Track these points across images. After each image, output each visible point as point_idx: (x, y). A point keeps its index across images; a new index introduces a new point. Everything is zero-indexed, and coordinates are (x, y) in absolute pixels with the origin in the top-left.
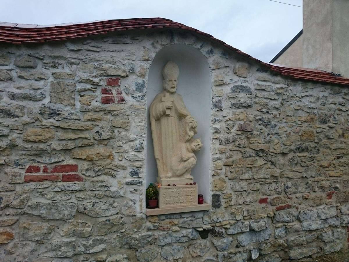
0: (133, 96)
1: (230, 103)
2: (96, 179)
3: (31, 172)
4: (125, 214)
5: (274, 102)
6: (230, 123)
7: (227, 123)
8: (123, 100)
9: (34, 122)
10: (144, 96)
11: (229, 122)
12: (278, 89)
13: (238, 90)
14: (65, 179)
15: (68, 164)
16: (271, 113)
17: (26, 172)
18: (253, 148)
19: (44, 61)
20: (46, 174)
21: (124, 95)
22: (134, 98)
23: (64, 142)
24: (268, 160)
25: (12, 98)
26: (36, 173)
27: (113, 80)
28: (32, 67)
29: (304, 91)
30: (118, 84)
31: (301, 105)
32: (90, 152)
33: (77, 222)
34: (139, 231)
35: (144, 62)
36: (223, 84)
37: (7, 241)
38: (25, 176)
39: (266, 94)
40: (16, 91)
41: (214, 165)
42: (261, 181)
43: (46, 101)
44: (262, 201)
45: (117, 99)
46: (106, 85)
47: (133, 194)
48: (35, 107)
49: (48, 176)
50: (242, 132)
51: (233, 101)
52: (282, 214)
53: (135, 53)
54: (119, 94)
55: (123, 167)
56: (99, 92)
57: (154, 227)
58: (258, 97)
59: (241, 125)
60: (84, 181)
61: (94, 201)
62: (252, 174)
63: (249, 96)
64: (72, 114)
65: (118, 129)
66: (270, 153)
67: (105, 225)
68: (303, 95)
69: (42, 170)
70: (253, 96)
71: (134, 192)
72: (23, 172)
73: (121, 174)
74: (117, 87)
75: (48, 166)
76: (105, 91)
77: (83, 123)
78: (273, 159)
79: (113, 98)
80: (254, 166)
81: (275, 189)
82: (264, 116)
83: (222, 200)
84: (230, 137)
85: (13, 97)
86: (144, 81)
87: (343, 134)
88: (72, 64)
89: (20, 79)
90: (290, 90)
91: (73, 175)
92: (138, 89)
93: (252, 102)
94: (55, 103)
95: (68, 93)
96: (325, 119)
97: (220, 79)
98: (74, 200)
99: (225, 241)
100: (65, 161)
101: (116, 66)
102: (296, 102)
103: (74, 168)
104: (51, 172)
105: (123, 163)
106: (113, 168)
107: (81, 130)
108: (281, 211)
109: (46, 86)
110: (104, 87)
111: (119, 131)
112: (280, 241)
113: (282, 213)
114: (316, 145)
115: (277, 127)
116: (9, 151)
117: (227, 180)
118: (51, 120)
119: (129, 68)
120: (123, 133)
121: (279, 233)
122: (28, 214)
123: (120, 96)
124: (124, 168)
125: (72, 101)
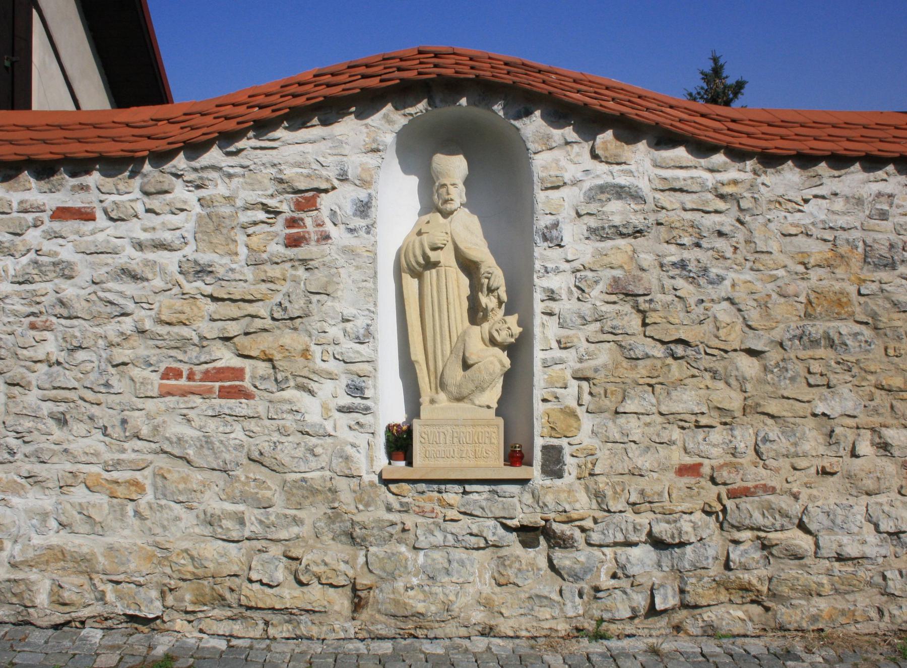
0: (349, 227)
1: (585, 227)
2: (279, 395)
3: (168, 379)
5: (716, 218)
6: (586, 276)
7: (578, 274)
8: (327, 237)
9: (170, 289)
10: (372, 225)
11: (583, 273)
12: (723, 184)
13: (604, 197)
14: (225, 393)
15: (228, 365)
16: (709, 246)
17: (162, 378)
18: (656, 337)
19: (185, 179)
20: (191, 383)
21: (329, 227)
22: (351, 231)
23: (219, 324)
24: (702, 368)
25: (138, 248)
26: (176, 379)
27: (305, 198)
28: (166, 192)
29: (807, 184)
30: (315, 206)
31: (802, 222)
32: (264, 343)
33: (247, 477)
34: (370, 509)
35: (370, 155)
36: (561, 184)
38: (161, 386)
39: (689, 200)
40: (144, 236)
42: (681, 420)
43: (189, 251)
44: (684, 470)
45: (314, 237)
46: (293, 209)
47: (353, 432)
48: (170, 261)
49: (196, 387)
50: (621, 296)
51: (593, 222)
52: (749, 506)
54: (319, 225)
55: (330, 374)
56: (279, 226)
57: (401, 504)
58: (663, 208)
59: (616, 280)
60: (257, 398)
61: (275, 439)
62: (654, 401)
63: (637, 207)
64: (232, 270)
65: (318, 297)
66: (708, 351)
67: (299, 488)
68: (808, 193)
69: (185, 374)
70: (651, 205)
72: (155, 377)
73: (325, 389)
74: (316, 212)
75: (196, 368)
76: (292, 223)
77: (252, 287)
78: (719, 366)
79: (307, 236)
80: (660, 380)
81: (724, 443)
82: (686, 255)
83: (568, 459)
84: (586, 309)
85: (140, 246)
86: (370, 194)
88: (230, 176)
89: (149, 215)
90: (760, 185)
91: (236, 386)
92: (358, 213)
93: (647, 222)
94: (204, 252)
95: (225, 231)
96: (888, 255)
97: (552, 173)
98: (239, 434)
99: (582, 559)
100: (223, 361)
101: (310, 172)
102: (788, 215)
103: (238, 373)
104: (201, 380)
105: (333, 366)
106: (311, 376)
107: (250, 301)
108: (744, 499)
109: (187, 223)
110: (289, 215)
111: (318, 301)
112: (741, 576)
113: (747, 503)
114: (857, 328)
115: (727, 283)
116: (135, 341)
117: (580, 411)
118: (199, 284)
119: (337, 172)
120: (329, 303)
121: (741, 555)
122: (166, 452)
123: (321, 229)
124: (332, 377)
125: (232, 246)
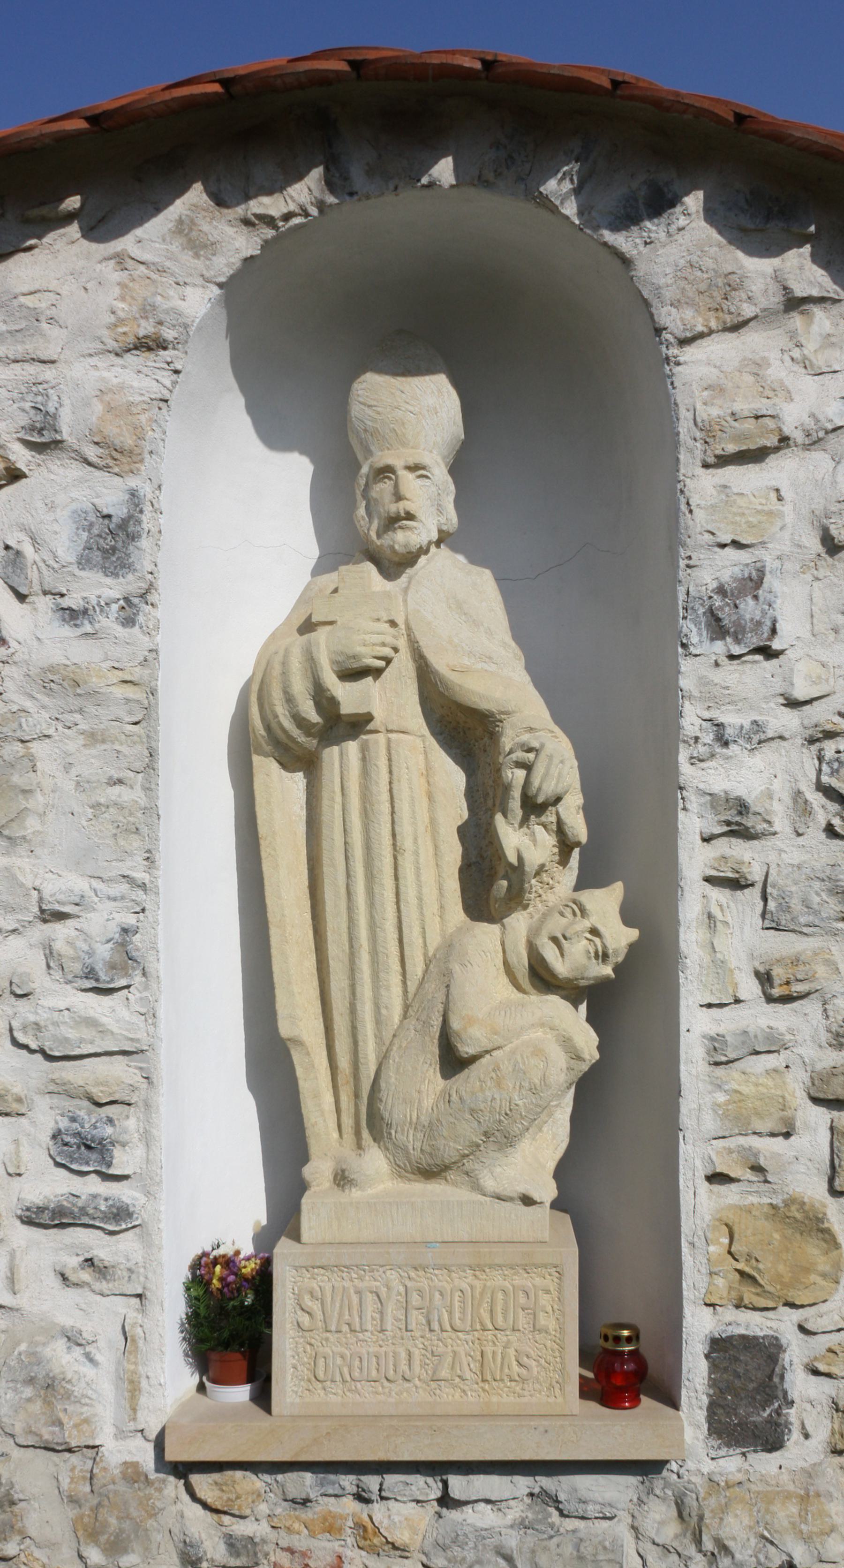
0: (65, 602)
4: (18, 1429)
35: (131, 359)
36: (772, 441)
37: (701, 1486)
41: (721, 1098)
47: (72, 1294)
53: (53, 312)
71: (86, 1276)
86: (133, 494)
87: (42, 429)
92: (97, 556)
97: (742, 406)
